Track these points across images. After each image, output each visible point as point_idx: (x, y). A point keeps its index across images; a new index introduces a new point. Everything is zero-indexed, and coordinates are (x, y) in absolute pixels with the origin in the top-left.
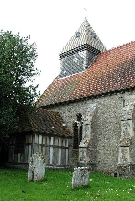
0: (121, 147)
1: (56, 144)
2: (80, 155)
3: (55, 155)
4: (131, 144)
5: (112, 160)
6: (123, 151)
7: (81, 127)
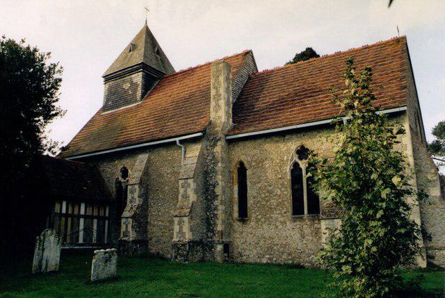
0: (176, 216)
1: (89, 213)
2: (123, 228)
3: (88, 230)
4: (190, 212)
5: (167, 234)
6: (180, 223)
7: (127, 186)
